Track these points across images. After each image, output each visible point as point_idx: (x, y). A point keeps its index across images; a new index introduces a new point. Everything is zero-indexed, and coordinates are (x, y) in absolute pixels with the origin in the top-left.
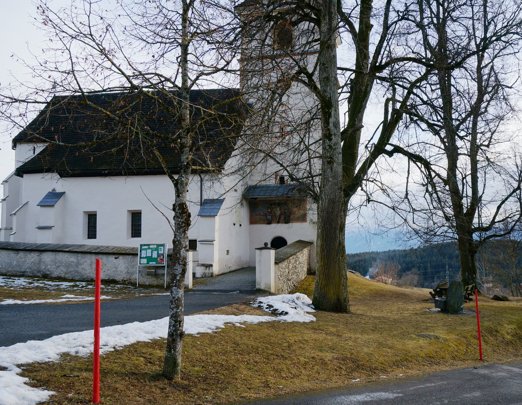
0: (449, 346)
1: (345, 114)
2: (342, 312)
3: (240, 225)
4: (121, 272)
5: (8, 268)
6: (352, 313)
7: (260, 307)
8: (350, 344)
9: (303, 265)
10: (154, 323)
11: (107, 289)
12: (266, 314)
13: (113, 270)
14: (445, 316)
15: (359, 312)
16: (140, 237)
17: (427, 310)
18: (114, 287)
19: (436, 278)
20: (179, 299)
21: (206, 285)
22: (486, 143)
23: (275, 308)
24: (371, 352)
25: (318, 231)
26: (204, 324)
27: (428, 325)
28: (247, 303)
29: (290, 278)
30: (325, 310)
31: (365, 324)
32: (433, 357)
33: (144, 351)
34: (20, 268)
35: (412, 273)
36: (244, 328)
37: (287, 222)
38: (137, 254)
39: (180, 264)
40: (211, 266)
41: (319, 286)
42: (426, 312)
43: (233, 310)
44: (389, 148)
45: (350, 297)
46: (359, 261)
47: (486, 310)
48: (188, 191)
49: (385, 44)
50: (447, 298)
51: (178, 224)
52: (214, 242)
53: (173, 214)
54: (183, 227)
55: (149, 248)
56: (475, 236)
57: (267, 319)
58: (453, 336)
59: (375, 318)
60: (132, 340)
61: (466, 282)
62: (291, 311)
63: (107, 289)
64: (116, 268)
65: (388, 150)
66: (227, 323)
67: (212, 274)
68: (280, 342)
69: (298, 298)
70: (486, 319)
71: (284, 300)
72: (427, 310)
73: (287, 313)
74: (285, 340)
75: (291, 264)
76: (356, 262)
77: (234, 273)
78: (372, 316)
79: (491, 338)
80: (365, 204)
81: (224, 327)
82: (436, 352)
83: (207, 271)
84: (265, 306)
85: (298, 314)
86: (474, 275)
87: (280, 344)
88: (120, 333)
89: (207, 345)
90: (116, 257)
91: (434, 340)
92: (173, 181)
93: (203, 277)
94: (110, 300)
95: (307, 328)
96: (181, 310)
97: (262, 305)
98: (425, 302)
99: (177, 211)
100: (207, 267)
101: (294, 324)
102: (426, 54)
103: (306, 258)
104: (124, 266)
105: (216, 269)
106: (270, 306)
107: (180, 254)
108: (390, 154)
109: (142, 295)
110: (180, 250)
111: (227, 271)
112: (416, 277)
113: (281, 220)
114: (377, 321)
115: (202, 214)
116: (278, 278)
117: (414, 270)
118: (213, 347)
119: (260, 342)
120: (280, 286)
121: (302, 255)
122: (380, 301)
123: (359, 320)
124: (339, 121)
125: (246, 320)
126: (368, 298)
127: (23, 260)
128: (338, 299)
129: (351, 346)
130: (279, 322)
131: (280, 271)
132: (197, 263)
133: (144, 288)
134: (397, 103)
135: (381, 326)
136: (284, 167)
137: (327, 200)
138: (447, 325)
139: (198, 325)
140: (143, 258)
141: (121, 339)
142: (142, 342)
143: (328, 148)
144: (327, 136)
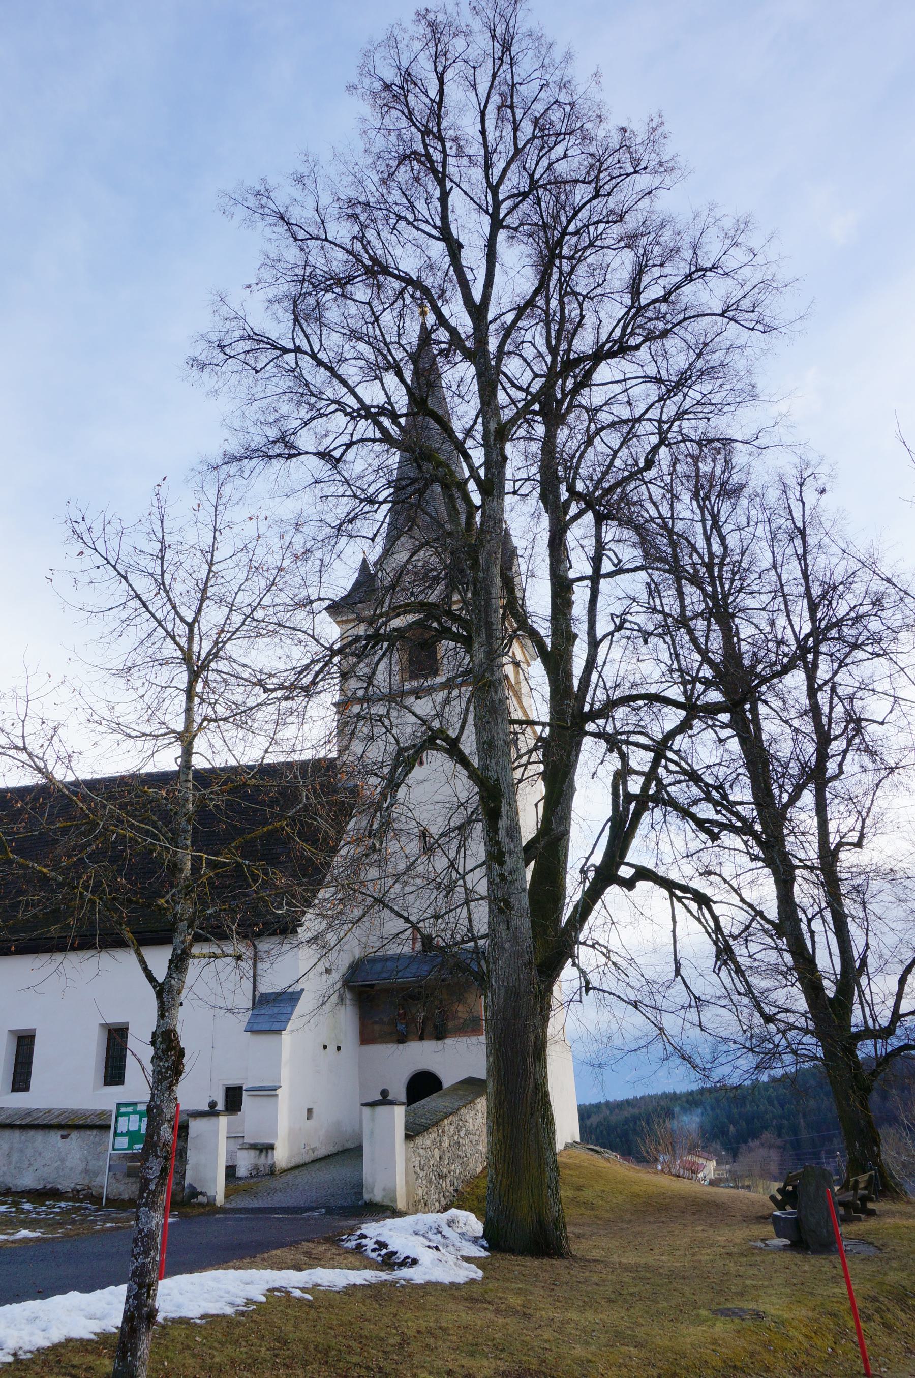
0: (790, 1339)
1: (536, 805)
2: (550, 1256)
3: (339, 1048)
4: (71, 1169)
5: (206, 682)
6: (574, 1258)
7: (359, 1246)
8: (545, 1337)
9: (476, 1138)
10: (111, 1293)
11: (38, 1213)
12: (371, 1265)
14: (798, 1258)
15: (596, 1254)
16: (122, 1083)
17: (760, 1244)
18: (54, 1207)
19: (823, 1155)
20: (151, 1235)
21: (255, 1195)
22: (854, 837)
23: (391, 1248)
24: (590, 1357)
25: (488, 1061)
26: (222, 1294)
27: (748, 1282)
28: (334, 1240)
29: (445, 1171)
30: (511, 1251)
31: (597, 1284)
32: (742, 1369)
33: (76, 1361)
35: (762, 1145)
36: (309, 1301)
37: (440, 1035)
38: (109, 1127)
39: (157, 1157)
40: (271, 1147)
41: (496, 1192)
42: (756, 1248)
43: (298, 1257)
44: (625, 872)
45: (571, 1214)
46: (635, 1119)
47: (901, 1238)
48: (181, 1004)
49: (594, 676)
50: (799, 1211)
51: (160, 1073)
52: (279, 1092)
53: (151, 1051)
54: (167, 1078)
55: (135, 1112)
56: (866, 1050)
57: (369, 1278)
58: (802, 1312)
59: (626, 1268)
60: (56, 1336)
61: (857, 1166)
62: (426, 1257)
63: (38, 1213)
64: (63, 1160)
65: (623, 875)
66: (275, 1289)
67: (272, 1167)
68: (382, 1335)
69: (451, 1223)
70: (894, 1264)
71: (417, 1228)
72: (760, 1244)
73: (415, 1262)
74: (396, 1328)
75: (446, 1138)
76: (626, 1121)
77: (323, 1163)
78: (620, 1263)
79: (902, 1315)
80: (577, 997)
81: (263, 1299)
82: (752, 1355)
83: (262, 1160)
84: (370, 1244)
85: (440, 1264)
86: (875, 1148)
87: (382, 1340)
88: (33, 1320)
89: (216, 1345)
91: (750, 1323)
92: (154, 987)
93: (251, 1176)
94: (38, 1239)
95: (455, 1298)
96: (154, 1258)
97: (364, 1241)
98: (760, 1223)
99: (158, 1046)
100: (261, 1150)
101: (431, 1287)
103: (485, 1121)
105: (282, 1156)
106: (382, 1245)
107: (158, 1135)
108: (629, 884)
109: (108, 1225)
110: (159, 1126)
111: (307, 1159)
112: (774, 1155)
114: (627, 1277)
115: (256, 1027)
116: (412, 1174)
117: (767, 1136)
118: (229, 1349)
119: (335, 1337)
120: (420, 1192)
121: (473, 1113)
122: (655, 1222)
123: (587, 1274)
124: (518, 824)
125: (319, 1282)
126: (628, 1217)
128: (541, 1223)
129: (546, 1341)
130: (394, 1283)
131: (420, 1156)
132: (240, 1141)
133: (118, 1208)
134: (634, 777)
135: (631, 1290)
136: (411, 922)
137: (503, 991)
138: (795, 1281)
139: (206, 1295)
140: (122, 1135)
141: (32, 1334)
142: (77, 1340)
143: (497, 880)
144: (495, 856)
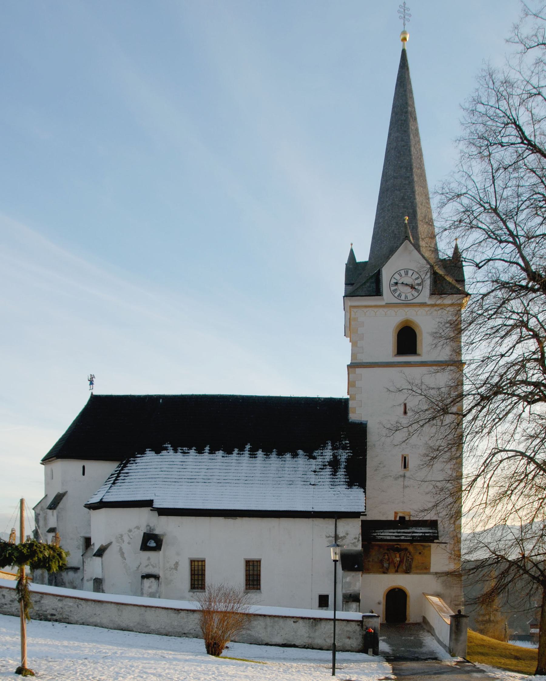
4: (301, 636)
13: (292, 634)
34: (183, 629)
37: (407, 571)
90: (295, 620)
102: (543, 433)
104: (304, 630)
113: (400, 569)
127: (185, 620)
